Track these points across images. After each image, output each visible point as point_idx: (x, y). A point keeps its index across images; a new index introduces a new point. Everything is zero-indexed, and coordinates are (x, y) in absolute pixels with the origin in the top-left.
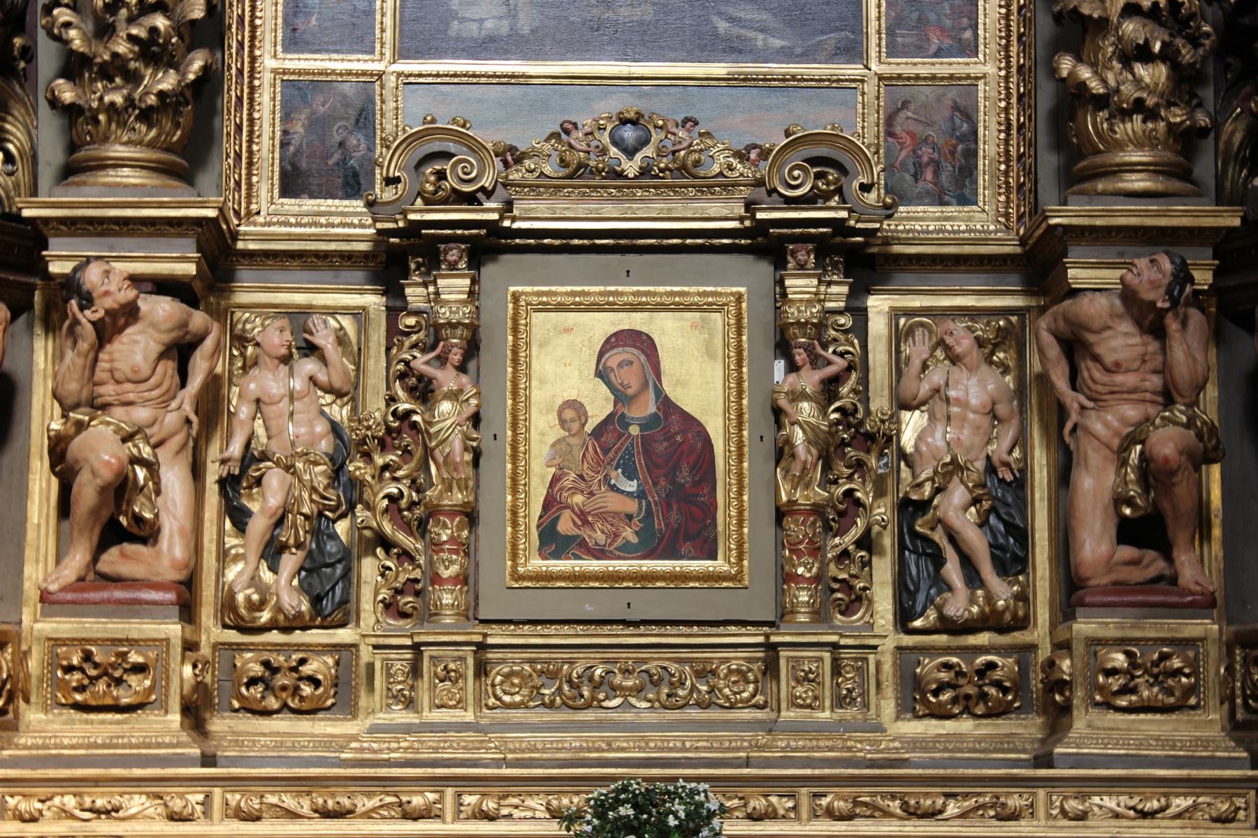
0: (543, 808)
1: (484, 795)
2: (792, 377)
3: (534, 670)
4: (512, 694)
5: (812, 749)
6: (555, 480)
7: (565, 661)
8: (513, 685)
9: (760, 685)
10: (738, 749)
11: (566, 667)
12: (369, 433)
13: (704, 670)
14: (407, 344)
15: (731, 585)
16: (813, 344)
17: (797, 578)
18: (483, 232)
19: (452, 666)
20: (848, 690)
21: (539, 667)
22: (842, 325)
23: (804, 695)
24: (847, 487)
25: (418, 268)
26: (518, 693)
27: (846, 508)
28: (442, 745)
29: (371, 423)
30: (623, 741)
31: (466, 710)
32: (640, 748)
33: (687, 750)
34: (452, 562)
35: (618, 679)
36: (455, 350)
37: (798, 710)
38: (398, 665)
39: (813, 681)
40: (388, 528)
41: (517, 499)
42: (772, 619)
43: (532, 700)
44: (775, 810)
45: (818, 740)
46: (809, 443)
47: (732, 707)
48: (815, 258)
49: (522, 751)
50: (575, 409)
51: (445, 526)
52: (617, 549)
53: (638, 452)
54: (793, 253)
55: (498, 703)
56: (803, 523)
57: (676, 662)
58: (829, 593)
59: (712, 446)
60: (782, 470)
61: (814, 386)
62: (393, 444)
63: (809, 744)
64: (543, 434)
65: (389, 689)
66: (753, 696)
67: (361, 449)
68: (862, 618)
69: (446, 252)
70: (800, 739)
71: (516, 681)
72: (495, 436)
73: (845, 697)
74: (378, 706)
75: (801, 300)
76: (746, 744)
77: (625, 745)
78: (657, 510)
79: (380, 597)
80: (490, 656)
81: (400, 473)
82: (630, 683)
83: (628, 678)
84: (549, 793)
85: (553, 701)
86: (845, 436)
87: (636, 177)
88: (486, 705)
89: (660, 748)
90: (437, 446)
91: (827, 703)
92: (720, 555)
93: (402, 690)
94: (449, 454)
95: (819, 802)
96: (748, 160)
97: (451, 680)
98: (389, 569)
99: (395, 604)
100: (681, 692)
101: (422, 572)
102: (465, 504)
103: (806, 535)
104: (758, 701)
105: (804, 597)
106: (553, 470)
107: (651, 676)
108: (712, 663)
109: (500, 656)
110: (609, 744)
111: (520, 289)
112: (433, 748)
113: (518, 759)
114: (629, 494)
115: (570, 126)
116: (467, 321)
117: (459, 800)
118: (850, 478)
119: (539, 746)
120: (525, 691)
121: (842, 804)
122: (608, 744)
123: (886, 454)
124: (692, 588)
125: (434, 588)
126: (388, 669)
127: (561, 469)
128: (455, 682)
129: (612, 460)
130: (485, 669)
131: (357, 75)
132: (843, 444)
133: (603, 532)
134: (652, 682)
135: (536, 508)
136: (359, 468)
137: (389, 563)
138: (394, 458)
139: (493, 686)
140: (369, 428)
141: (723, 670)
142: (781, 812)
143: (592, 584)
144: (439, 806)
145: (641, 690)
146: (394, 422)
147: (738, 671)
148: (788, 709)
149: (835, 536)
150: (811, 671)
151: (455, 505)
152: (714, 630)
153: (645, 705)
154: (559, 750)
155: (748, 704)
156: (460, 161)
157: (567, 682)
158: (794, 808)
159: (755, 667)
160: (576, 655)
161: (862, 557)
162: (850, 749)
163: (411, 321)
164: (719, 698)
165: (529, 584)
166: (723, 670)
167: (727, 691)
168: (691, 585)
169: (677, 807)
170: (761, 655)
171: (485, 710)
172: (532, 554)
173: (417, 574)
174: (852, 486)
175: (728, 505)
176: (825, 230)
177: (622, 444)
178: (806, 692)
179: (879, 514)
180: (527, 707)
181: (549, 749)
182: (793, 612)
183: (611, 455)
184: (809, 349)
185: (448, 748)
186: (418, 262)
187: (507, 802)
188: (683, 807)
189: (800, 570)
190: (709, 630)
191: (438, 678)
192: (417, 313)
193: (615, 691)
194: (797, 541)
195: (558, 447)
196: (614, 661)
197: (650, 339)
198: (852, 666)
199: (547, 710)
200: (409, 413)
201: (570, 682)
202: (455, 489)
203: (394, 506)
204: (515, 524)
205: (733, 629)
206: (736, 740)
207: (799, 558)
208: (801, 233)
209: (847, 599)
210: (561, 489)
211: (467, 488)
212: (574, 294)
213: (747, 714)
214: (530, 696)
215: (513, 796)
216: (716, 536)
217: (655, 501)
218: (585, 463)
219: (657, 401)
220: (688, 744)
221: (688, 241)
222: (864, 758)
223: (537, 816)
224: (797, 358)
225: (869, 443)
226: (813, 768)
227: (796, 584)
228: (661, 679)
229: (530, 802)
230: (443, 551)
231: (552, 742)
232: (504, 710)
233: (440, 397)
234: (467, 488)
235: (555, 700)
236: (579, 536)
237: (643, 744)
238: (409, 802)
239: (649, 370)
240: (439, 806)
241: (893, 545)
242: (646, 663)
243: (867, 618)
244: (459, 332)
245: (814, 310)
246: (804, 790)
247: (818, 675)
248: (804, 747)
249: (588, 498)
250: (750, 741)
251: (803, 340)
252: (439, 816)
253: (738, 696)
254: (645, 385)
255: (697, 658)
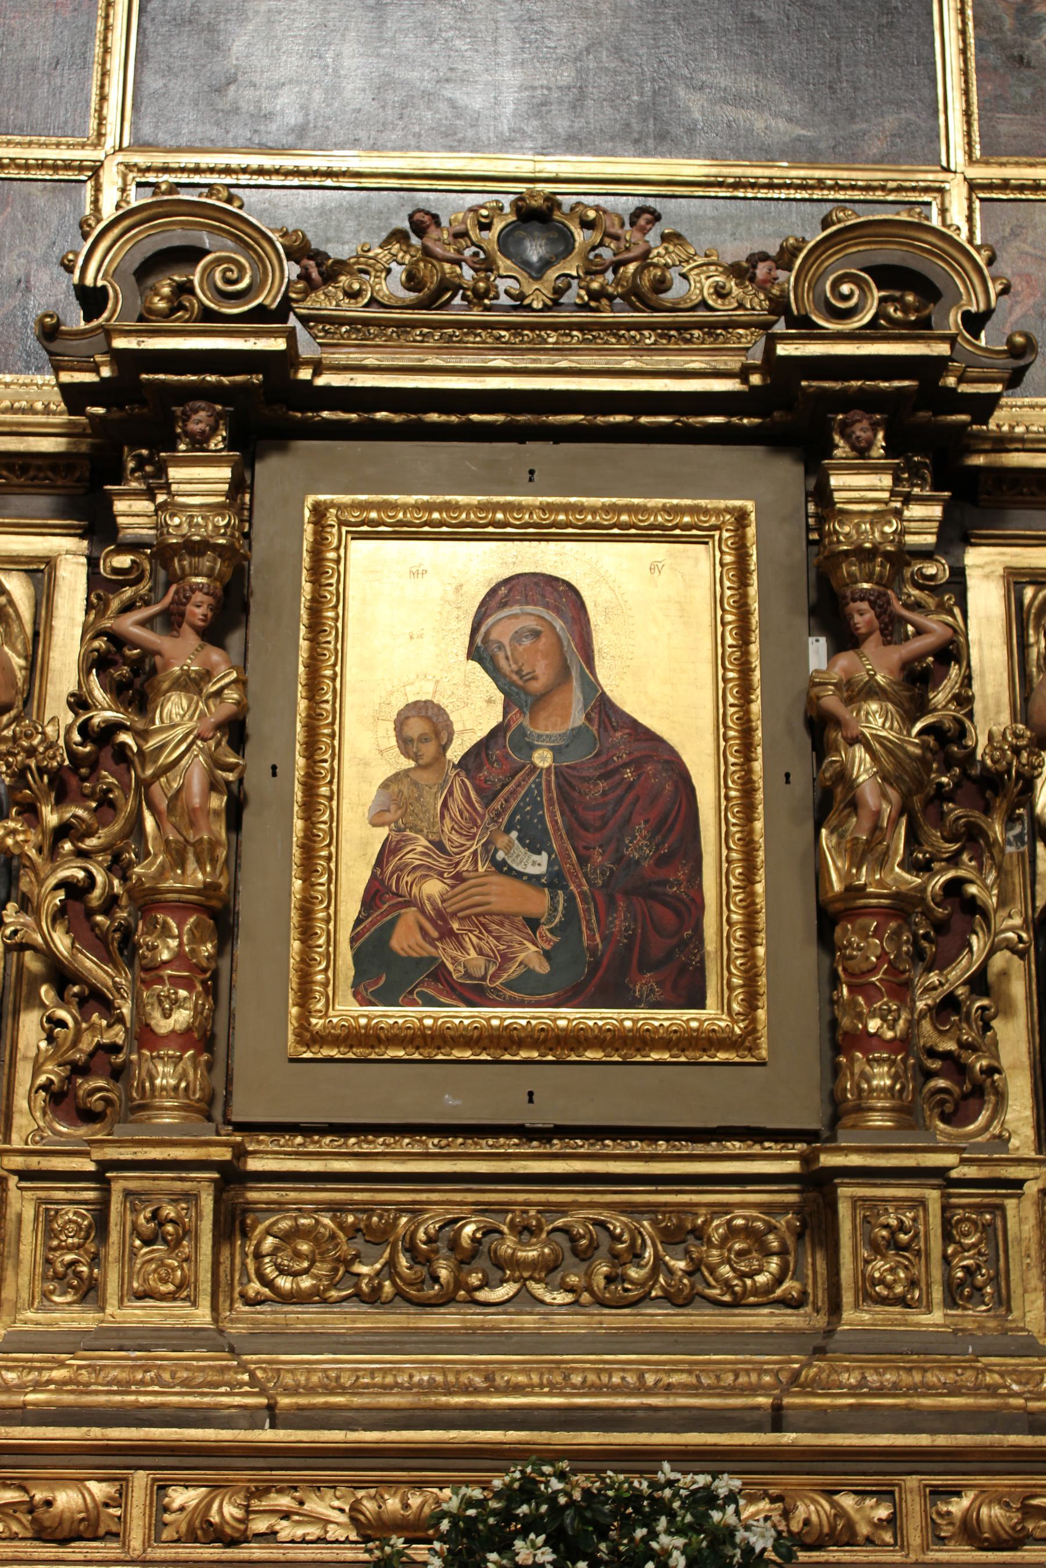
0: (343, 1518)
1: (215, 1487)
2: (845, 660)
3: (341, 1226)
4: (295, 1274)
5: (913, 1390)
6: (387, 851)
7: (402, 1208)
8: (298, 1255)
9: (791, 1259)
10: (753, 1390)
11: (404, 1220)
12: (33, 763)
13: (680, 1227)
14: (115, 604)
15: (732, 1057)
16: (885, 594)
17: (867, 1041)
18: (257, 379)
19: (169, 1211)
20: (966, 1269)
21: (351, 1219)
22: (932, 577)
23: (889, 1278)
24: (950, 875)
25: (139, 467)
26: (306, 1271)
27: (950, 915)
28: (139, 1376)
29: (35, 742)
30: (520, 1372)
31: (194, 1304)
32: (551, 1385)
33: (649, 1392)
34: (176, 1003)
35: (508, 1246)
36: (198, 597)
37: (878, 1308)
38: (70, 1213)
39: (906, 1248)
40: (62, 942)
41: (313, 885)
42: (815, 1126)
43: (334, 1286)
44: (850, 1525)
45: (925, 1370)
46: (883, 779)
47: (737, 1303)
48: (885, 438)
49: (311, 1390)
50: (429, 719)
51: (165, 932)
52: (508, 985)
53: (550, 801)
54: (845, 430)
55: (266, 1291)
56: (877, 933)
57: (623, 1212)
58: (920, 1079)
59: (693, 790)
60: (832, 832)
61: (891, 672)
62: (81, 788)
63: (905, 1379)
64: (367, 764)
65: (48, 1262)
66: (779, 1281)
67: (19, 796)
68: (986, 1128)
69: (186, 418)
70: (886, 1369)
71: (304, 1247)
72: (274, 768)
73: (962, 1283)
74: (25, 1295)
75: (863, 513)
76: (767, 1379)
77: (521, 1379)
78: (587, 911)
79: (42, 1079)
80: (252, 1196)
81: (92, 842)
82: (532, 1254)
83: (528, 1244)
84: (357, 1485)
85: (377, 1290)
86: (945, 780)
87: (546, 308)
88: (243, 1296)
89: (592, 1386)
90: (156, 776)
91: (937, 1294)
92: (711, 999)
93: (74, 1263)
94: (179, 790)
95: (944, 1508)
96: (752, 279)
97: (166, 1242)
98: (62, 1024)
99: (71, 1094)
100: (633, 1273)
101: (127, 1031)
102: (210, 888)
103: (882, 956)
104: (788, 1291)
105: (882, 1078)
106: (383, 832)
107: (574, 1239)
108: (696, 1215)
109: (273, 1196)
110: (489, 1378)
111: (322, 497)
112: (119, 1383)
113: (300, 1408)
114: (533, 880)
115: (426, 218)
116: (221, 541)
117: (160, 1499)
118: (954, 860)
119: (347, 1380)
120: (322, 1269)
121: (997, 1511)
122: (487, 1379)
123: (1020, 816)
124: (656, 1063)
125: (140, 1055)
126: (49, 1221)
127: (399, 830)
128: (174, 1245)
129: (499, 815)
130: (243, 1223)
131: (55, 168)
132: (941, 795)
133: (480, 952)
134: (575, 1252)
135: (350, 907)
136: (13, 832)
137: (62, 1014)
138: (80, 812)
139: (258, 1256)
140: (31, 752)
141: (717, 1229)
142: (864, 1530)
143: (457, 1054)
144: (116, 1512)
145: (555, 1268)
146: (82, 744)
147: (748, 1231)
148: (856, 1306)
149: (929, 970)
150: (902, 1228)
151: (188, 891)
152: (700, 1149)
153: (562, 1298)
154: (387, 1389)
155: (766, 1298)
156: (219, 261)
157: (406, 1250)
158: (891, 1522)
159: (781, 1222)
160: (423, 1197)
161: (983, 1008)
162: (992, 1390)
163: (124, 561)
164: (709, 1286)
165: (334, 1053)
166: (717, 1229)
167: (725, 1270)
168: (655, 1056)
169: (664, 1539)
170: (792, 1198)
171: (239, 1306)
172: (340, 993)
173: (117, 1035)
174: (961, 873)
175: (725, 901)
176: (906, 383)
177: (519, 785)
178: (892, 1271)
179: (1012, 929)
180: (325, 1301)
181: (367, 1386)
182: (861, 1109)
183: (497, 805)
184: (879, 604)
185: (152, 1383)
186: (140, 456)
187: (265, 1503)
188: (680, 1541)
189: (873, 1025)
190: (687, 1148)
191: (139, 1236)
192: (134, 547)
193: (503, 1269)
194: (865, 967)
195: (395, 788)
196: (500, 1209)
197: (572, 590)
198: (974, 1223)
199: (365, 1308)
200: (113, 728)
201: (411, 1249)
202: (191, 865)
203: (76, 907)
204: (307, 934)
205: (735, 1146)
206: (747, 1372)
207: (869, 1002)
208: (860, 388)
209: (956, 1090)
210: (400, 869)
211: (214, 861)
212: (430, 507)
213: (765, 1319)
214: (331, 1278)
215: (280, 1491)
216: (702, 961)
217: (582, 893)
218: (447, 820)
219: (585, 706)
220: (650, 1379)
221: (643, 420)
222: (1024, 1408)
223: (330, 1536)
224: (857, 618)
225: (989, 794)
226: (933, 1432)
227: (865, 1053)
228: (593, 1246)
229: (315, 1505)
230: (160, 980)
231: (372, 1372)
232: (278, 1307)
233: (165, 685)
234: (214, 861)
235: (381, 1286)
236: (433, 959)
237: (559, 1379)
238: (49, 1503)
239: (571, 645)
240: (116, 1512)
241: (1029, 997)
242: (564, 1213)
243: (995, 1129)
244: (206, 562)
245: (887, 529)
246: (912, 1482)
247: (916, 1235)
248: (895, 1386)
249: (453, 887)
250: (776, 1374)
251: (866, 586)
252: (116, 1535)
253: (749, 1282)
254: (564, 673)
255: (666, 1204)
